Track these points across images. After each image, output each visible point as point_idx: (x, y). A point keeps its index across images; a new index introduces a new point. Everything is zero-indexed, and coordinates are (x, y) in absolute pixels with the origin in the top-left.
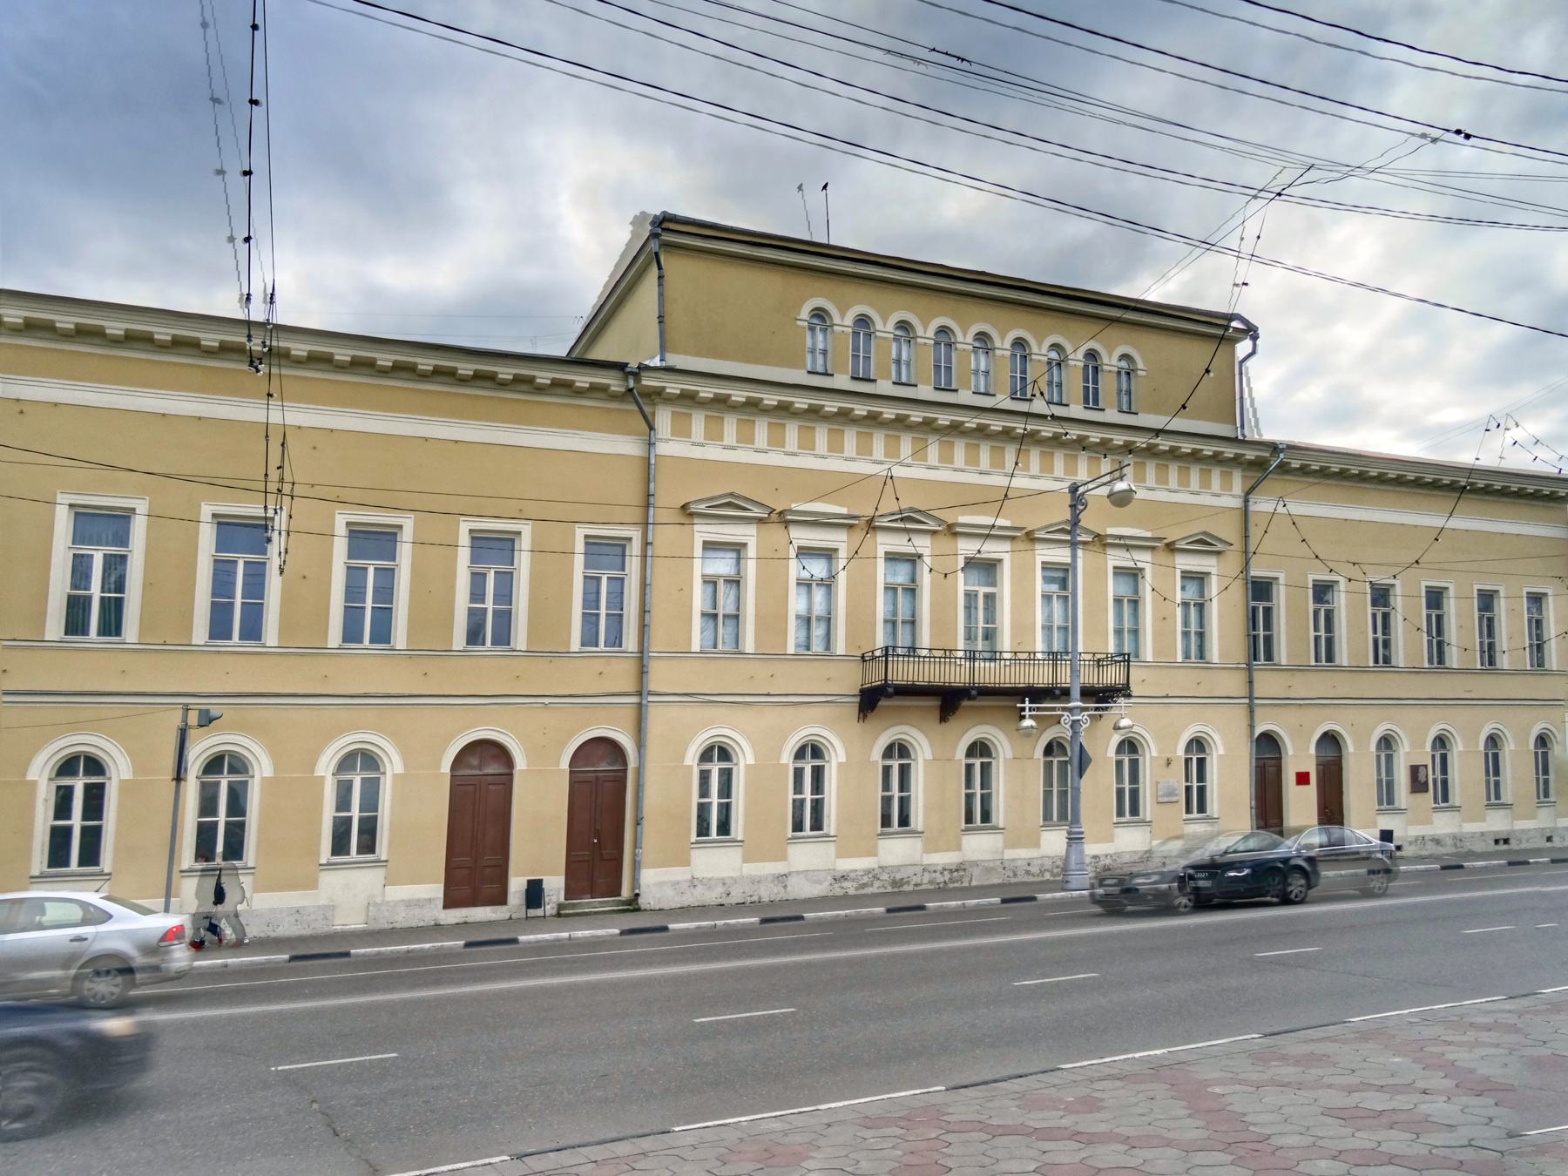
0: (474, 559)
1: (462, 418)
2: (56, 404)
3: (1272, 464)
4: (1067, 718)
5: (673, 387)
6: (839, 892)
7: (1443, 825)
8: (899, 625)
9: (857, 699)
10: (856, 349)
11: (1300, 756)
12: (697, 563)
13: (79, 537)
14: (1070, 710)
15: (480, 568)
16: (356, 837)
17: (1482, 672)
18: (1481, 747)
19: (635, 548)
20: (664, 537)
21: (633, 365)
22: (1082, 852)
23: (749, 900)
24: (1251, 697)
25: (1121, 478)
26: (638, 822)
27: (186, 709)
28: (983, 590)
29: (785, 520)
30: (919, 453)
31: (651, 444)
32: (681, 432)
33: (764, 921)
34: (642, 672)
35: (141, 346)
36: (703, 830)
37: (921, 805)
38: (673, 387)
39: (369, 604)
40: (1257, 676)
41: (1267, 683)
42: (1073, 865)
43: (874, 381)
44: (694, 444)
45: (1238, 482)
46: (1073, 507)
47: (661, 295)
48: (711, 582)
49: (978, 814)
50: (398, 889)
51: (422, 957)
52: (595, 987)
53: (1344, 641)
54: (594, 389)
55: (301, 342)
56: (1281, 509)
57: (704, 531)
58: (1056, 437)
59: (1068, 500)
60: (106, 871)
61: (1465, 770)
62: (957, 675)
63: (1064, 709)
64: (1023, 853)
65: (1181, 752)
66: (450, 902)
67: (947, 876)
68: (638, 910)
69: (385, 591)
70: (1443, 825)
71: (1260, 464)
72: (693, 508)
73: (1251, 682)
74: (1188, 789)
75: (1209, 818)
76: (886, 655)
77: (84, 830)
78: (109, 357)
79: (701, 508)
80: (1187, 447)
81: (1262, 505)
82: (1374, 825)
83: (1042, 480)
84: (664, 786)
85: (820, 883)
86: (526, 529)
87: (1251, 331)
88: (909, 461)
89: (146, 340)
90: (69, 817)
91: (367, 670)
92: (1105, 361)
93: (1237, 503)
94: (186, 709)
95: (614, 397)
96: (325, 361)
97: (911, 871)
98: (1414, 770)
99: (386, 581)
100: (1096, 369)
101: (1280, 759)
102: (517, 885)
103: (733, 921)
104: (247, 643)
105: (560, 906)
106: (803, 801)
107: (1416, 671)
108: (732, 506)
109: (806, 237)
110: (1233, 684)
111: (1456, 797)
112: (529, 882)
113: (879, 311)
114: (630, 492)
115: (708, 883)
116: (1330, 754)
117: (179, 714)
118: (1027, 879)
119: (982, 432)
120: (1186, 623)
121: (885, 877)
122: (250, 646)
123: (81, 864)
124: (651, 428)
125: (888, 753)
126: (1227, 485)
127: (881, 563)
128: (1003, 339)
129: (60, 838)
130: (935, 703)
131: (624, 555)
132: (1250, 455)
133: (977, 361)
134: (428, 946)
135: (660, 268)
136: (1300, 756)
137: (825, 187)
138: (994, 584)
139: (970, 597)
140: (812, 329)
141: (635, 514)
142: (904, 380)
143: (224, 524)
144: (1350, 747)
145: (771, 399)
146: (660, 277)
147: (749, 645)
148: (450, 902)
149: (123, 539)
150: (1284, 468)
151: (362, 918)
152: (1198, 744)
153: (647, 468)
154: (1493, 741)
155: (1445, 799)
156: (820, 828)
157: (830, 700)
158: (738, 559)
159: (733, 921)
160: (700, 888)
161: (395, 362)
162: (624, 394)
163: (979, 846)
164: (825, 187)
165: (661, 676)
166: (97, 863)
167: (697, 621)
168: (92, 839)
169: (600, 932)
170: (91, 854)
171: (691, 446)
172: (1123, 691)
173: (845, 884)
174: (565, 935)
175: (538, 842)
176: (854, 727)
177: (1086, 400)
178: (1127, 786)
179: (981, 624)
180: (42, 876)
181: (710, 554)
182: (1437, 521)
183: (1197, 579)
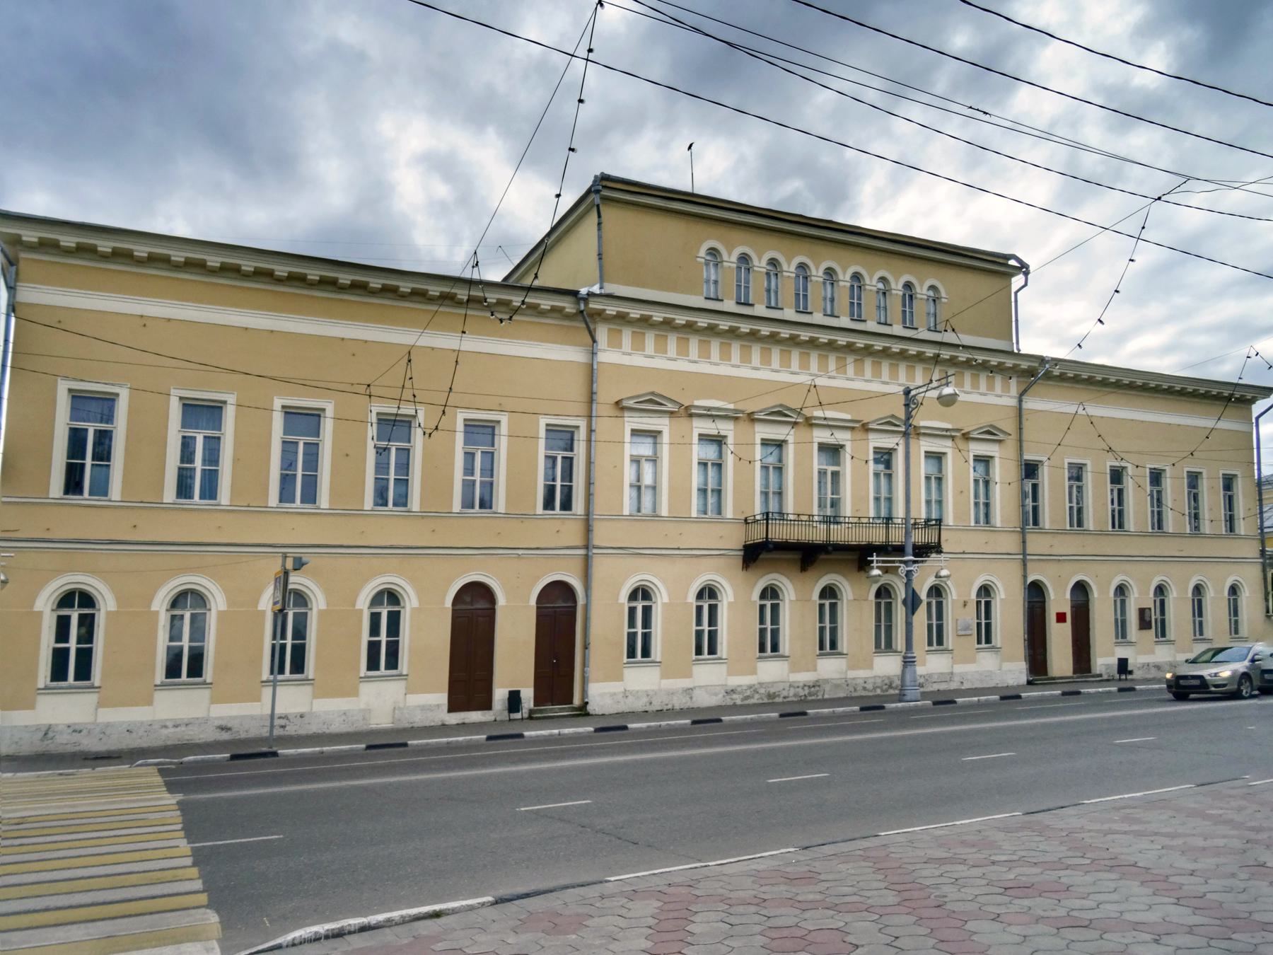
0: (467, 442)
1: (366, 321)
2: (169, 320)
3: (1038, 373)
4: (903, 569)
5: (611, 309)
6: (729, 703)
7: (1162, 654)
8: (771, 495)
9: (742, 553)
10: (739, 280)
11: (1059, 600)
12: (627, 446)
13: (75, 413)
14: (905, 562)
15: (470, 449)
16: (382, 656)
17: (1191, 536)
18: (1190, 595)
19: (581, 435)
20: (603, 426)
21: (584, 291)
22: (915, 672)
23: (665, 708)
24: (1024, 554)
25: (947, 384)
26: (586, 647)
27: (285, 556)
28: (831, 469)
29: (689, 413)
30: (877, 374)
31: (593, 354)
32: (615, 344)
33: (694, 722)
34: (588, 530)
35: (297, 284)
36: (631, 654)
37: (787, 638)
38: (611, 309)
39: (300, 473)
40: (1029, 537)
41: (1037, 544)
42: (908, 683)
43: (752, 305)
44: (624, 354)
45: (1014, 386)
46: (907, 405)
47: (600, 237)
48: (636, 461)
49: (769, 644)
50: (414, 697)
51: (450, 748)
52: (686, 760)
53: (1091, 510)
54: (555, 310)
55: (282, 264)
56: (1081, 411)
57: (633, 421)
58: (968, 361)
59: (902, 400)
60: (97, 684)
61: (1178, 612)
62: (817, 534)
63: (901, 562)
64: (862, 674)
65: (973, 596)
66: (453, 707)
67: (807, 691)
68: (588, 714)
69: (212, 455)
70: (1162, 654)
71: (1031, 373)
72: (625, 404)
73: (1024, 542)
74: (979, 625)
75: (993, 647)
76: (767, 519)
77: (79, 651)
78: (137, 274)
79: (631, 403)
80: (963, 356)
81: (1030, 404)
82: (1113, 655)
83: (880, 386)
84: (604, 621)
85: (716, 695)
86: (504, 419)
87: (1023, 268)
88: (834, 374)
89: (165, 261)
90: (67, 641)
91: (390, 528)
92: (918, 290)
93: (1013, 402)
94: (285, 556)
95: (569, 317)
96: (200, 266)
97: (781, 687)
98: (1142, 612)
99: (213, 446)
100: (911, 297)
101: (1044, 602)
102: (500, 695)
103: (672, 722)
104: (306, 506)
105: (531, 712)
106: (765, 629)
107: (1101, 533)
108: (653, 403)
109: (683, 185)
110: (1010, 543)
111: (1172, 633)
112: (511, 692)
113: (727, 247)
114: (576, 390)
115: (636, 694)
116: (1081, 598)
117: (280, 561)
118: (864, 693)
119: (712, 330)
120: (976, 496)
121: (762, 691)
122: (308, 508)
123: (76, 679)
124: (594, 341)
125: (763, 596)
126: (1006, 388)
127: (758, 448)
128: (789, 265)
129: (60, 658)
130: (854, 556)
131: (493, 435)
132: (1024, 365)
133: (708, 271)
134: (460, 739)
135: (599, 216)
136: (1059, 600)
137: (690, 147)
138: (838, 464)
139: (822, 473)
140: (707, 264)
141: (581, 409)
142: (773, 304)
143: (289, 412)
144: (1095, 593)
145: (681, 319)
146: (599, 224)
147: (664, 511)
148: (453, 707)
149: (109, 418)
150: (1048, 376)
151: (390, 720)
152: (985, 590)
153: (591, 373)
154: (1198, 590)
155: (1163, 635)
156: (395, 667)
157: (722, 554)
158: (655, 443)
159: (672, 722)
160: (631, 699)
161: (290, 273)
162: (575, 315)
163: (830, 668)
164: (690, 147)
165: (601, 535)
166: (200, 676)
167: (627, 489)
168: (85, 658)
169: (580, 730)
170: (84, 672)
171: (627, 358)
172: (937, 548)
173: (734, 696)
174: (556, 731)
175: (514, 665)
176: (739, 573)
177: (904, 322)
178: (934, 622)
179: (829, 496)
180: (46, 688)
181: (637, 439)
182: (1209, 423)
183: (984, 461)
